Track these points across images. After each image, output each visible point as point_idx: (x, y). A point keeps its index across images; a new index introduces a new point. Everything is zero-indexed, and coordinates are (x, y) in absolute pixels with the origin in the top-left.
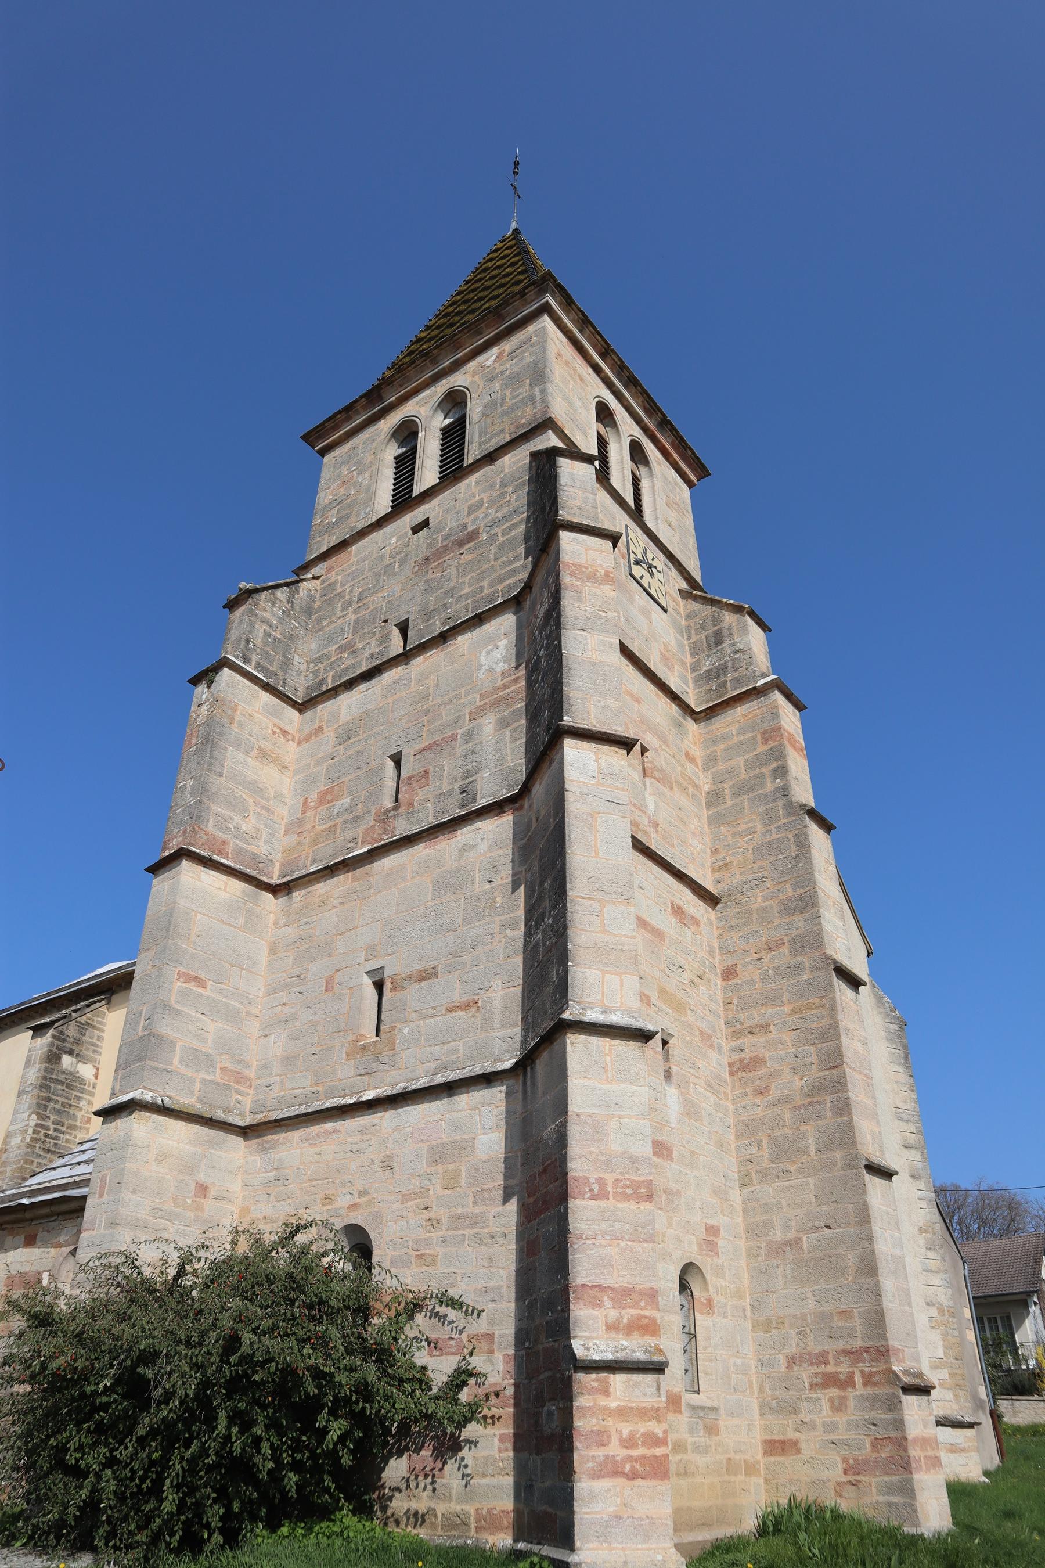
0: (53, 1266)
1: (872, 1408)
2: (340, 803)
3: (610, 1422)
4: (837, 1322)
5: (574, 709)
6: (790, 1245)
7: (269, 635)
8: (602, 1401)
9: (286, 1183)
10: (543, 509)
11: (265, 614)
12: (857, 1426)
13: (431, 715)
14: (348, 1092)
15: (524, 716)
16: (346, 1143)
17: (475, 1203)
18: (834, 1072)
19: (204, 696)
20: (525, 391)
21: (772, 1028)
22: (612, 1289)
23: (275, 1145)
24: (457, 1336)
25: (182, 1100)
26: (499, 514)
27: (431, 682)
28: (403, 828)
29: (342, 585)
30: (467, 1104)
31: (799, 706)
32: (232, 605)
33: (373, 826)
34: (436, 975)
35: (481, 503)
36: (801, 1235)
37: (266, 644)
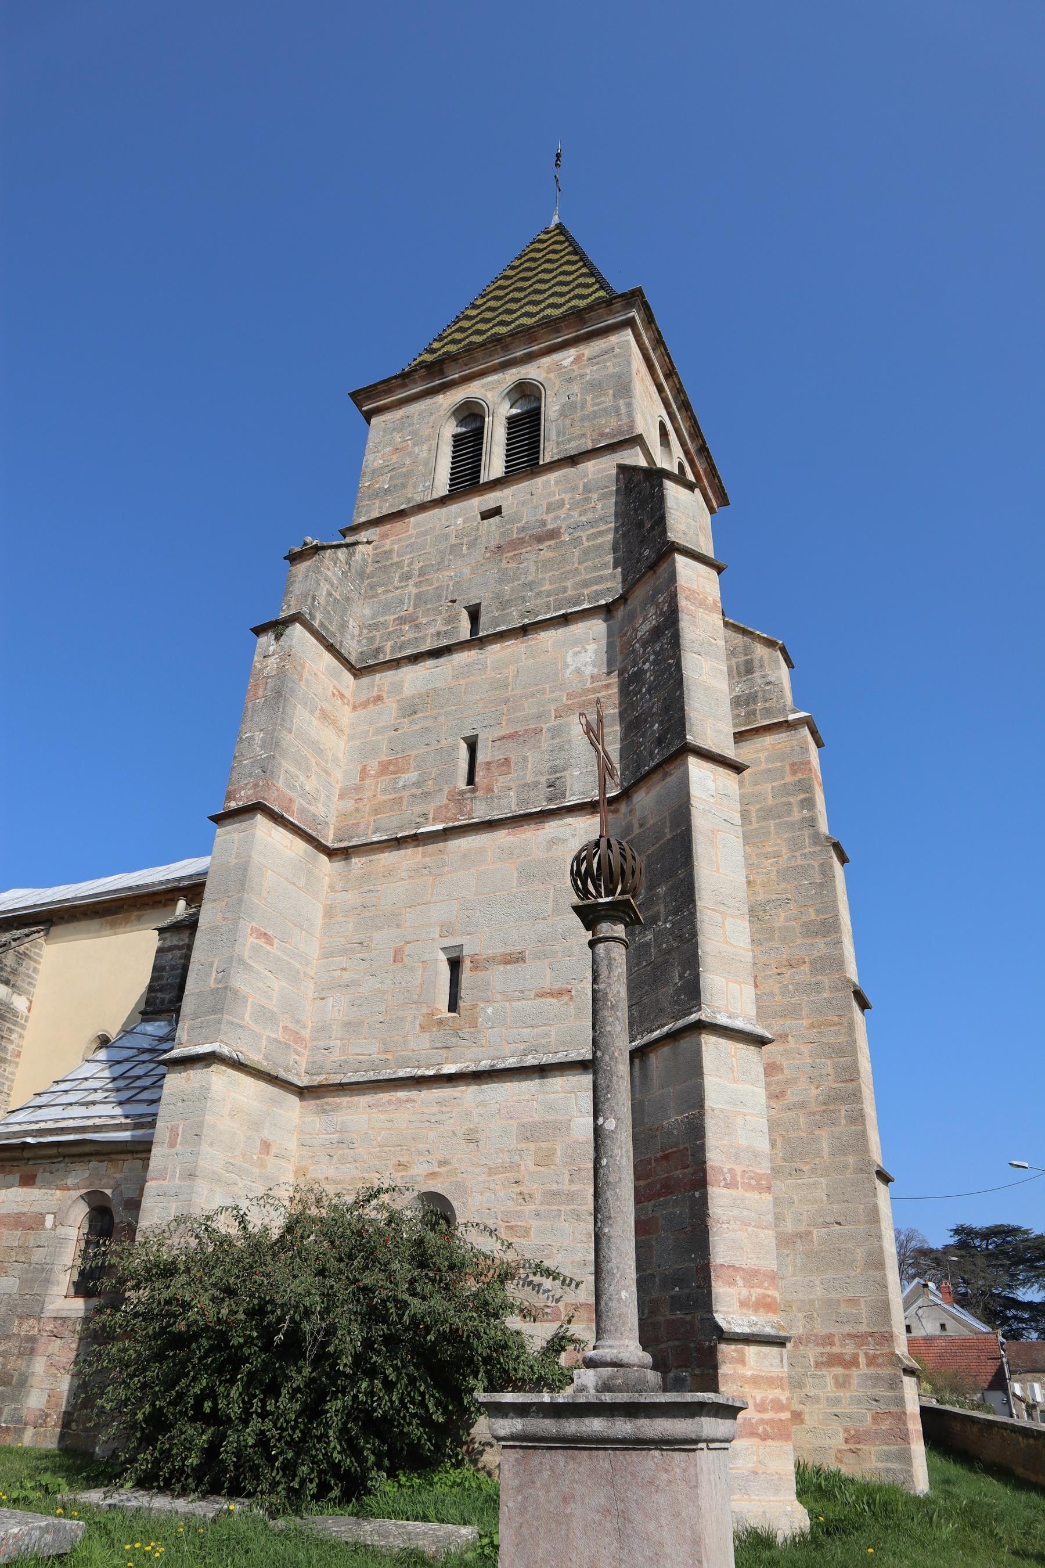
0: (60, 1209)
1: (874, 1386)
2: (406, 776)
3: (747, 1389)
4: (844, 1309)
5: (694, 729)
6: (801, 1237)
7: (331, 595)
8: (741, 1370)
9: (351, 1146)
10: (640, 525)
11: (329, 573)
12: (859, 1401)
13: (511, 704)
14: (422, 1063)
15: (618, 723)
16: (423, 1113)
17: (571, 1181)
18: (850, 1085)
19: (271, 648)
20: (608, 400)
21: (790, 1038)
22: (743, 1269)
23: (337, 1108)
24: (554, 1304)
25: (251, 1056)
26: (584, 519)
27: (511, 670)
28: (481, 812)
30: (562, 1087)
31: (819, 744)
32: (294, 558)
33: (446, 806)
34: (523, 960)
35: (562, 504)
36: (811, 1229)
37: (328, 602)
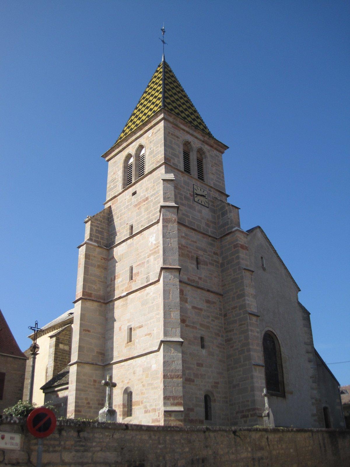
29: (116, 210)
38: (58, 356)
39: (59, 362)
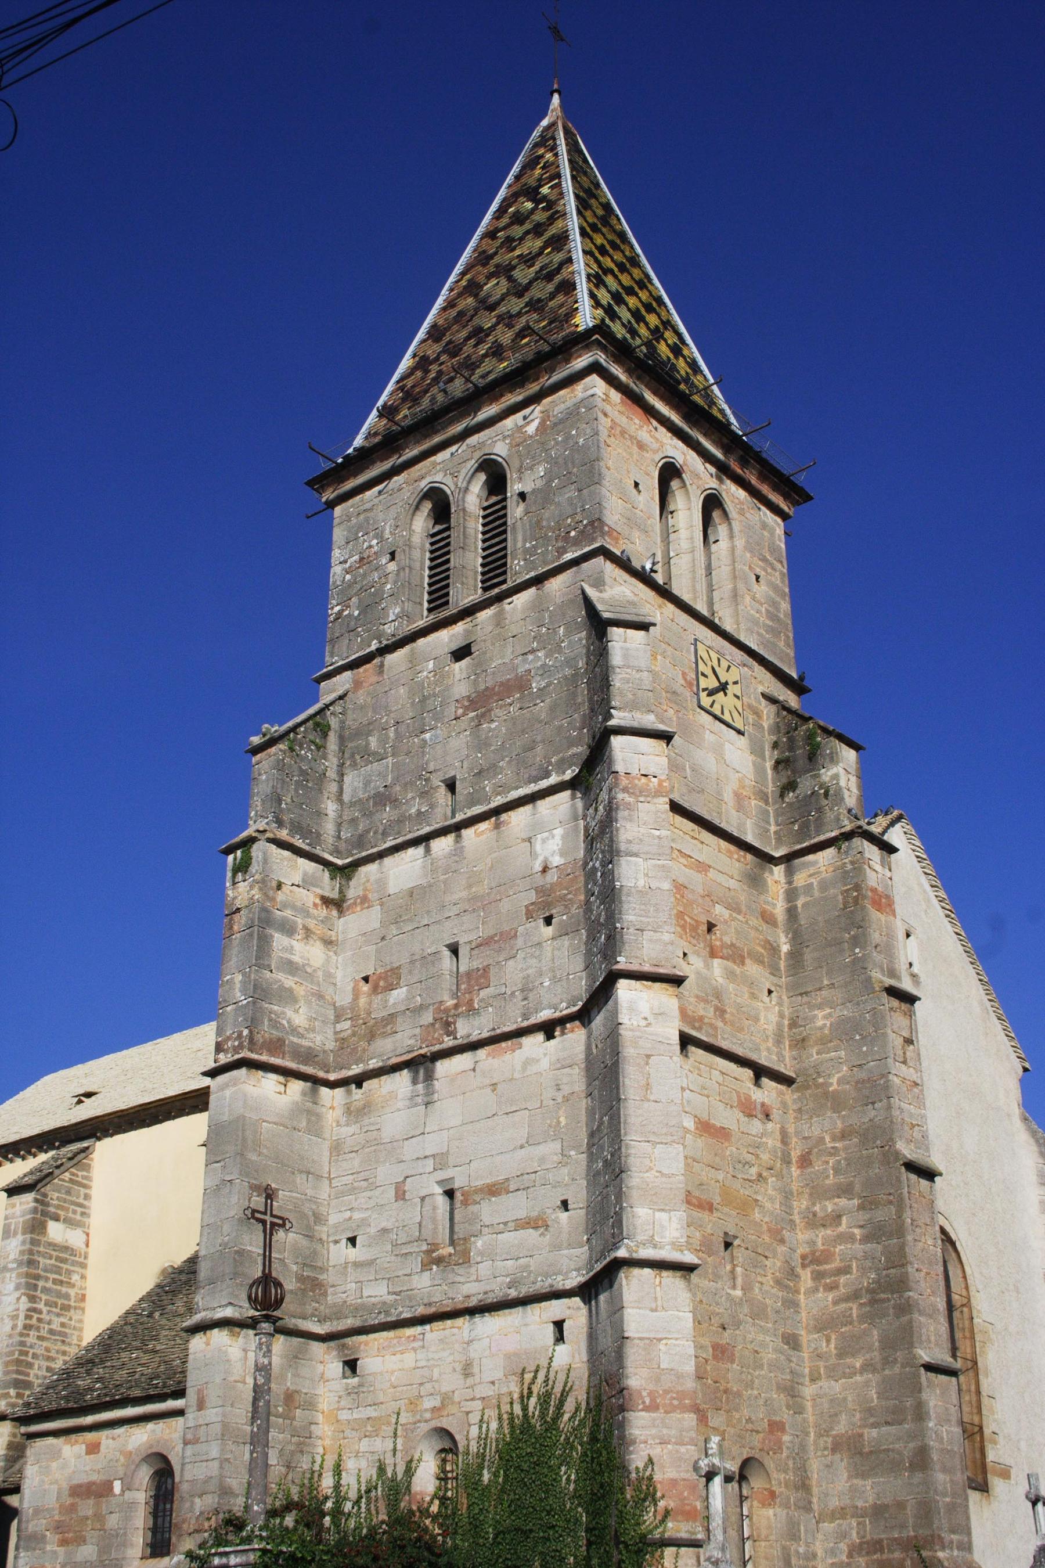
0: (125, 1474)
38: (42, 1273)
39: (44, 1297)
